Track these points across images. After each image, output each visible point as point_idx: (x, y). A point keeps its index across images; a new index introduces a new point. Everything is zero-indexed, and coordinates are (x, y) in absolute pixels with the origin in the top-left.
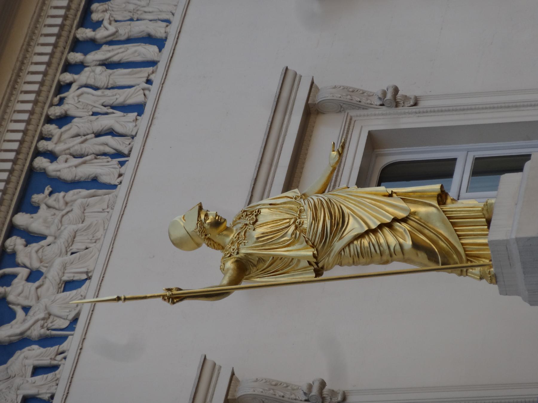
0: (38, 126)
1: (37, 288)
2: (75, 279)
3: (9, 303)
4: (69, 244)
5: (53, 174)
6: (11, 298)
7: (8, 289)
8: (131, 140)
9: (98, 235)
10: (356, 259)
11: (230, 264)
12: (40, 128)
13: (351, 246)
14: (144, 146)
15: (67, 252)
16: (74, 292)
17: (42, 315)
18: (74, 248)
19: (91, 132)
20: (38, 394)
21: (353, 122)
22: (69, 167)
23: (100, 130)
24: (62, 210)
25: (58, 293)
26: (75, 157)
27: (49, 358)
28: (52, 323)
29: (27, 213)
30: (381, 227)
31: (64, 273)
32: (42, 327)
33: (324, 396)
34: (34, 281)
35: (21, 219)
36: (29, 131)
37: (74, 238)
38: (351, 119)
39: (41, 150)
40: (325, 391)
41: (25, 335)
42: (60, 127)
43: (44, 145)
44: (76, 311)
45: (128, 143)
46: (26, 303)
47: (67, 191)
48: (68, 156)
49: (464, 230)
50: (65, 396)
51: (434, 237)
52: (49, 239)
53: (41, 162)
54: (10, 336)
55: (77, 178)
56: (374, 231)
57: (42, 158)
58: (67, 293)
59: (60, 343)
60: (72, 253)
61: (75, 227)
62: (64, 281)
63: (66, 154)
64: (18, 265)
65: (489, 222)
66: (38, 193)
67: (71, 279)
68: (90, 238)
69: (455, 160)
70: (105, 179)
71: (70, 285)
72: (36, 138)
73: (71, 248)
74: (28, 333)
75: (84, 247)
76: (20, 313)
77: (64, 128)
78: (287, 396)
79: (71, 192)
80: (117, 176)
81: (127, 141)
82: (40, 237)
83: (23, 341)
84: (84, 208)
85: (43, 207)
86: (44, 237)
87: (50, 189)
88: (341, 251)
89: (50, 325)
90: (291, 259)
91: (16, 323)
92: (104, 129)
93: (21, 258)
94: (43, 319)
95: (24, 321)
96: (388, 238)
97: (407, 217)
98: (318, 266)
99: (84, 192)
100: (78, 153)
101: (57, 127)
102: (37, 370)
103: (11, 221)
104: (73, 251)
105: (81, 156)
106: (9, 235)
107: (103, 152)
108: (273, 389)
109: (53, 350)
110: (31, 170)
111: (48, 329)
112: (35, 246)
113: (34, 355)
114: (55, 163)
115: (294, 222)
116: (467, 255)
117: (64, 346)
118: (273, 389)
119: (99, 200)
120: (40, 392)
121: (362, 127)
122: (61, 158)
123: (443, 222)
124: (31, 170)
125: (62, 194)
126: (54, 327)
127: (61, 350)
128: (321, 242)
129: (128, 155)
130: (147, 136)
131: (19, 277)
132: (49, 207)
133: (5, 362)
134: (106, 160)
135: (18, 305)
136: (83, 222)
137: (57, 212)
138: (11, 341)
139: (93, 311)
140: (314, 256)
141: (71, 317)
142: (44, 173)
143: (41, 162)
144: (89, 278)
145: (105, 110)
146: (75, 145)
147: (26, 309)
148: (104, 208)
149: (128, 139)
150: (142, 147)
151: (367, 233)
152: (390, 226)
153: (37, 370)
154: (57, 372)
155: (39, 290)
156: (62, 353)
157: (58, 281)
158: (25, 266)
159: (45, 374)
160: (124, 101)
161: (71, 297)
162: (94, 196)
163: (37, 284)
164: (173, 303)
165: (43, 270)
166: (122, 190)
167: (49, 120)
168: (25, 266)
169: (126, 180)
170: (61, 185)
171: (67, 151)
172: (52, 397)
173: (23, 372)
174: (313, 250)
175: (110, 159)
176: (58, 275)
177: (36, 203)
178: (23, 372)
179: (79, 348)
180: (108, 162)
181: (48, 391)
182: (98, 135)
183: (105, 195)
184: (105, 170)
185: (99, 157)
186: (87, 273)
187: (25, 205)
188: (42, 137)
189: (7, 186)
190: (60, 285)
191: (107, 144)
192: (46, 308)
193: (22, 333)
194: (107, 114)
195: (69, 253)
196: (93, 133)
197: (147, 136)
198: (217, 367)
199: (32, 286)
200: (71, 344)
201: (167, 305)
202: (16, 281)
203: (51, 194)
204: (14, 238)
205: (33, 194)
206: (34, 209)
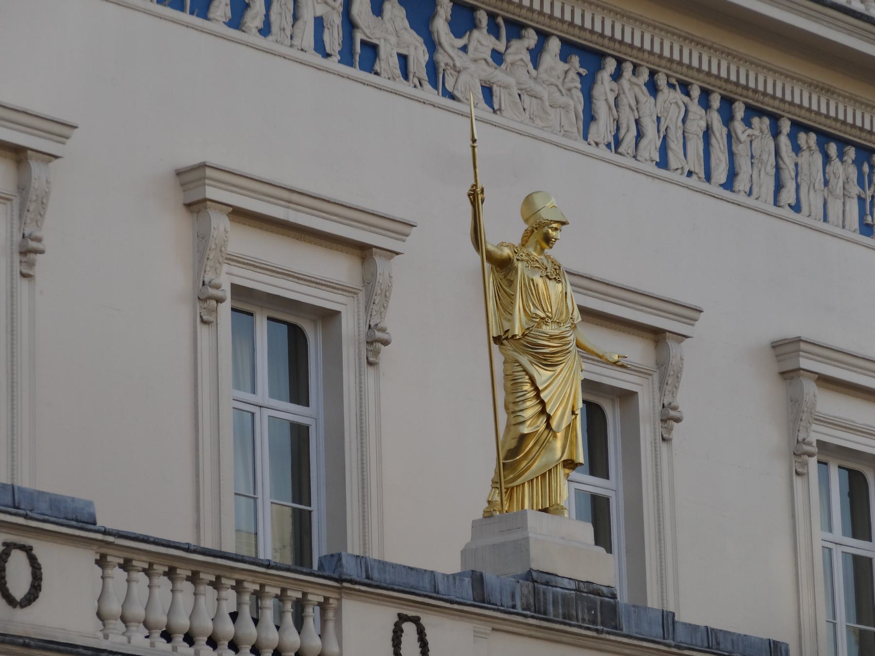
1: (485, 60)
2: (494, 98)
3: (471, 32)
5: (599, 77)
6: (476, 34)
7: (485, 31)
10: (510, 378)
11: (507, 252)
12: (645, 64)
17: (458, 64)
30: (542, 403)
32: (447, 64)
34: (492, 57)
35: (554, 45)
41: (438, 47)
43: (628, 68)
46: (471, 48)
47: (582, 90)
51: (531, 457)
52: (534, 73)
53: (611, 65)
54: (438, 32)
55: (594, 101)
56: (538, 396)
58: (480, 88)
59: (430, 82)
60: (519, 95)
61: (546, 98)
65: (545, 510)
66: (580, 62)
70: (593, 128)
74: (441, 50)
75: (525, 107)
76: (460, 42)
77: (644, 89)
78: (374, 307)
80: (597, 140)
81: (631, 151)
83: (432, 45)
84: (565, 107)
85: (566, 67)
86: (536, 67)
87: (584, 74)
89: (448, 72)
93: (516, 44)
94: (454, 66)
95: (453, 47)
96: (530, 410)
99: (580, 108)
100: (620, 103)
102: (403, 59)
103: (553, 34)
106: (539, 32)
109: (424, 75)
110: (603, 55)
112: (527, 57)
115: (548, 316)
116: (512, 488)
117: (427, 86)
119: (572, 122)
122: (614, 85)
123: (545, 465)
124: (603, 55)
125: (579, 86)
128: (528, 343)
131: (497, 42)
132: (566, 72)
140: (514, 336)
141: (457, 93)
142: (600, 67)
143: (611, 65)
144: (495, 112)
145: (663, 129)
146: (628, 99)
147: (464, 49)
153: (403, 59)
154: (402, 79)
155: (484, 62)
157: (493, 81)
158: (507, 48)
160: (671, 149)
163: (490, 60)
165: (503, 66)
166: (582, 145)
167: (653, 73)
168: (507, 48)
169: (592, 150)
171: (621, 92)
172: (377, 73)
175: (613, 134)
182: (637, 122)
184: (602, 129)
186: (500, 109)
187: (569, 48)
188: (636, 66)
192: (466, 68)
193: (440, 44)
194: (659, 131)
199: (488, 55)
201: (467, 189)
203: (579, 74)
204: (536, 37)
206: (564, 57)
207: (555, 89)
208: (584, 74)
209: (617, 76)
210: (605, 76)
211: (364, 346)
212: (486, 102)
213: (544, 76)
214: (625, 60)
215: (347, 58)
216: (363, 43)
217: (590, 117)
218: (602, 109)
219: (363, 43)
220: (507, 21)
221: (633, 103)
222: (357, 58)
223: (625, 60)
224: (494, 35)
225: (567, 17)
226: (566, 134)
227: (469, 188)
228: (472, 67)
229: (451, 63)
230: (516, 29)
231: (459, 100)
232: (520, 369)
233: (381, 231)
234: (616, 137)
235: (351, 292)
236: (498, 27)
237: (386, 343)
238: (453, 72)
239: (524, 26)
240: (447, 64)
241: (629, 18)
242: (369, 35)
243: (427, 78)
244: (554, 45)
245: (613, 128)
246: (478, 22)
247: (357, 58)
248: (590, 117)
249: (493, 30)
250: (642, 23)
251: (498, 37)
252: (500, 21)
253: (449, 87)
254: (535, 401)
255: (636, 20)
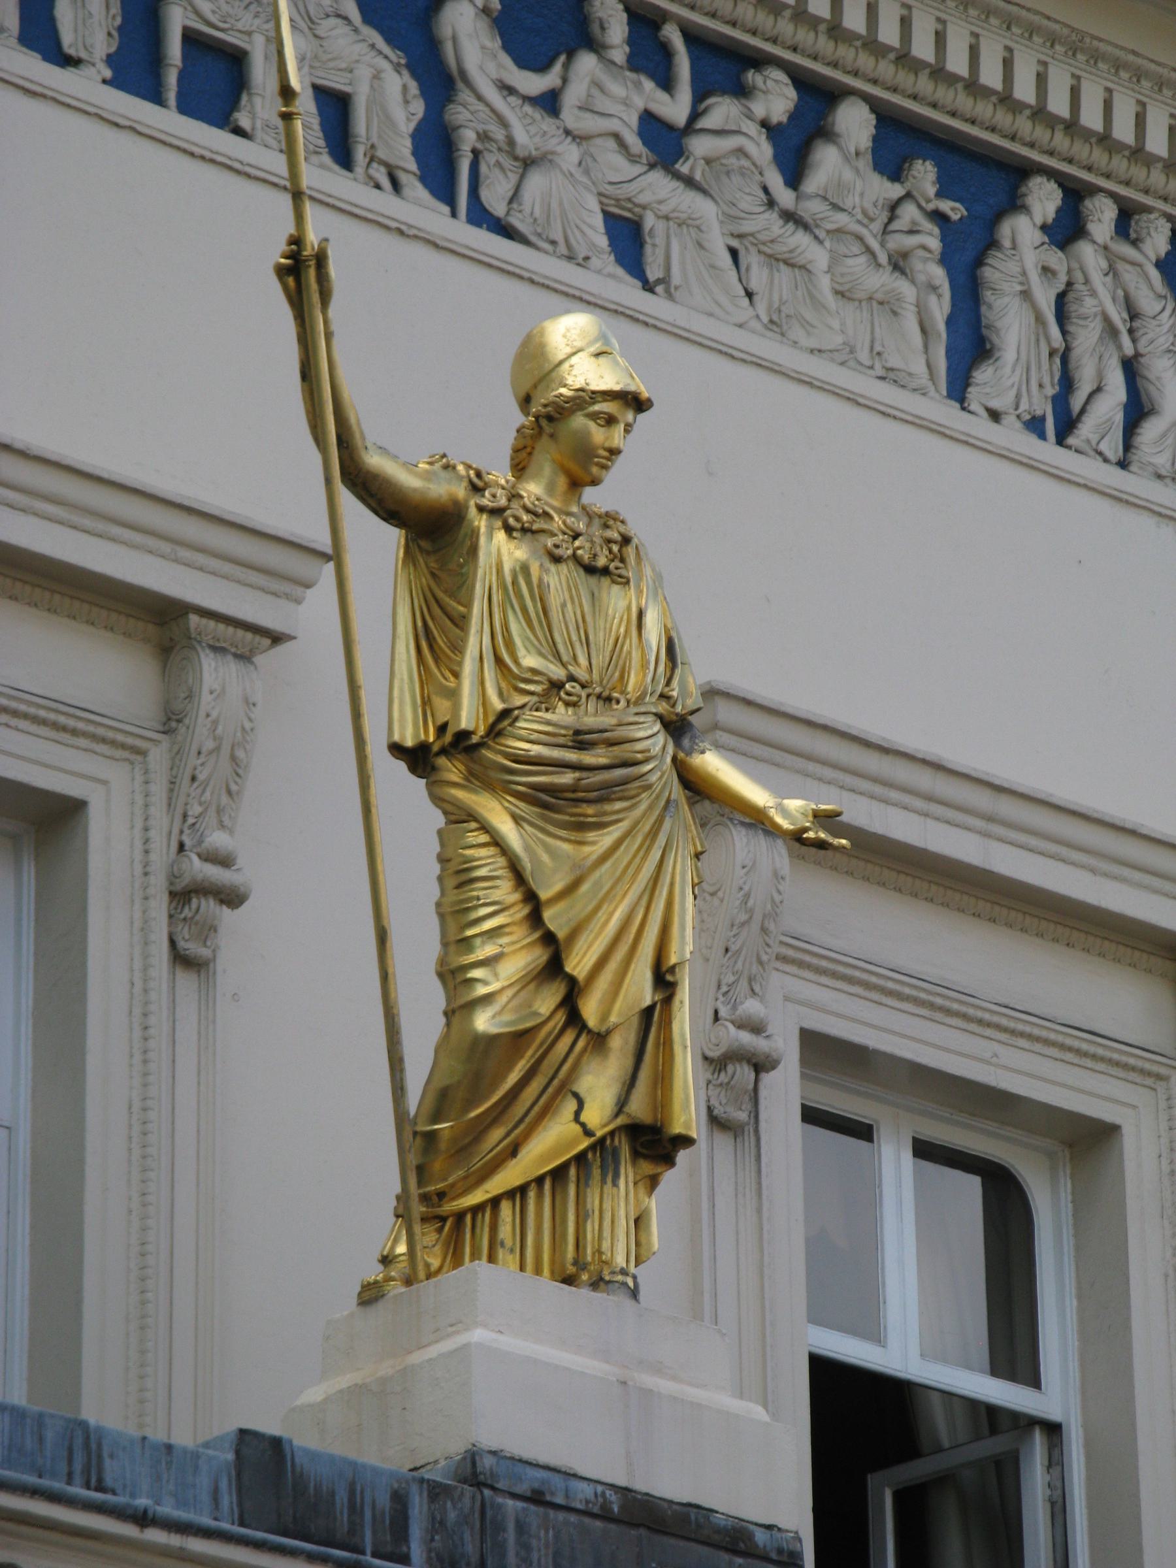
0: (1165, 199)
1: (617, 137)
2: (648, 249)
3: (571, 54)
4: (764, 244)
5: (1005, 230)
6: (586, 62)
8: (1113, 458)
9: (796, 333)
10: (453, 866)
11: (447, 490)
12: (1160, 205)
13: (492, 851)
14: (1085, 486)
15: (740, 236)
16: (603, 241)
17: (521, 136)
18: (751, 259)
19: (1142, 350)
20: (250, 94)
21: (1149, 1081)
22: (1024, 273)
23: (1146, 373)
24: (883, 244)
25: (600, 194)
26: (1061, 301)
27: (375, 140)
28: (498, 164)
29: (875, 139)
31: (667, 218)
32: (484, 137)
33: (195, 901)
34: (642, 134)
35: (854, 123)
36: (1144, 171)
37: (786, 263)
38: (1159, 1077)
39: (1088, 203)
40: (209, 906)
41: (460, 85)
42: (1159, 265)
43: (1102, 218)
44: (533, 238)
45: (1103, 447)
47: (945, 260)
48: (1063, 278)
49: (540, 1208)
50: (237, 165)
51: (519, 1109)
52: (785, 196)
53: (1044, 200)
54: (455, 39)
55: (988, 295)
56: (535, 918)
57: (1059, 202)
58: (598, 221)
59: (423, 179)
60: (734, 253)
62: (641, 217)
63: (1069, 272)
64: (701, 95)
66: (940, 179)
67: (648, 239)
68: (783, 308)
69: (1035, 1382)
70: (983, 375)
71: (627, 238)
72: (1123, 191)
73: (753, 250)
74: (465, 95)
75: (754, 285)
76: (534, 83)
77: (1155, 274)
79: (939, 274)
80: (994, 404)
81: (1112, 446)
82: (794, 169)
83: (438, 79)
84: (888, 305)
85: (895, 191)
87: (955, 217)
88: (476, 820)
90: (456, 668)
91: (500, 66)
92: (1151, 388)
93: (722, 111)
94: (511, 142)
97: (583, 1027)
98: (438, 754)
99: (940, 309)
100: (1072, 308)
101: (1163, 254)
102: (335, 107)
103: (849, 92)
104: (742, 253)
105: (1062, 316)
106: (802, 81)
107: (1077, 377)
108: (217, 749)
109: (403, 153)
110: (1019, 172)
111: (476, 153)
112: (762, 150)
113: (389, 103)
114: (1039, 237)
115: (572, 678)
116: (460, 1216)
117: (416, 190)
118: (217, 749)
119: (919, 354)
120: (258, 101)
121: (1134, 1107)
122: (1055, 258)
124: (1019, 172)
125: (935, 244)
126: (483, 169)
127: (403, 178)
128: (507, 756)
129: (1061, 441)
130: (1120, 500)
131: (662, 96)
132: (893, 208)
133: (369, 17)
134: (1046, 380)
135: (565, 80)
136: (840, 294)
137: (877, 226)
138: (440, 42)
139: (532, 281)
140: (463, 735)
141: (516, 221)
142: (1014, 204)
143: (1044, 200)
144: (648, 287)
146: (1099, 300)
147: (550, 103)
148: (885, 355)
149: (1116, 451)
150: (1082, 481)
151: (531, 897)
152: (554, 968)
153: (335, 107)
154: (326, 159)
155: (611, 144)
156: (396, 185)
157: (642, 199)
158: (695, 116)
159: (322, 124)
161: (589, 232)
162: (924, 331)
163: (635, 143)
164: (282, 272)
166: (946, 413)
169: (981, 427)
170: (969, 255)
171: (1078, 276)
172: (239, 131)
173: (331, 64)
174: (482, 731)
175: (1050, 391)
176: (660, 202)
177: (909, 170)
178: (331, 64)
179: (403, 227)
180: (1041, 386)
181: (259, 124)
182: (1131, 368)
183: (929, 366)
184: (1015, 371)
185: (1058, 361)
186: (664, 281)
187: (901, 140)
188: (1127, 216)
189: (960, 86)
190: (630, 205)
191: (1098, 390)
193: (463, 74)
195: (735, 243)
196: (1137, 355)
197: (1120, 500)
198: (298, 591)
199: (628, 125)
200: (419, 208)
201: (276, 252)
202: (648, 85)
203: (938, 217)
204: (792, 93)
205: (937, 165)
206: (890, 159)
207: (856, 248)
208: (955, 217)
209: (1067, 230)
210: (1023, 232)
211: (160, 907)
212: (620, 261)
213: (812, 208)
214: (1093, 190)
215: (136, 69)
216: (191, 38)
217: (971, 346)
218: (1013, 326)
219: (191, 38)
220: (694, 38)
221: (1118, 317)
222: (172, 78)
223: (1093, 190)
224: (652, 76)
225: (889, 34)
226: (889, 376)
227: (283, 247)
228: (570, 153)
229: (499, 134)
230: (727, 66)
231: (524, 240)
232: (484, 838)
233: (215, 564)
234: (1061, 401)
235: (123, 746)
236: (666, 52)
237: (232, 898)
238: (507, 162)
239: (759, 61)
240: (484, 137)
241: (1096, 57)
242: (213, 19)
243: (413, 166)
244: (854, 123)
245: (1048, 376)
246: (595, 29)
247: (172, 78)
248: (971, 346)
249: (649, 58)
250: (1139, 75)
251: (667, 83)
252: (672, 34)
253: (495, 198)
254: (520, 936)
255: (1118, 66)
